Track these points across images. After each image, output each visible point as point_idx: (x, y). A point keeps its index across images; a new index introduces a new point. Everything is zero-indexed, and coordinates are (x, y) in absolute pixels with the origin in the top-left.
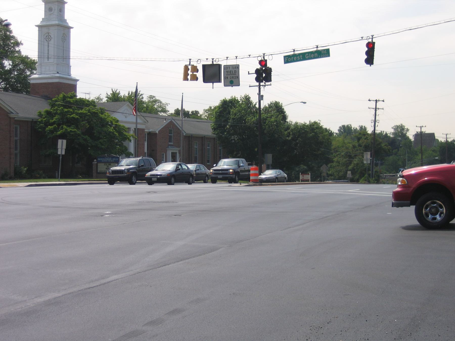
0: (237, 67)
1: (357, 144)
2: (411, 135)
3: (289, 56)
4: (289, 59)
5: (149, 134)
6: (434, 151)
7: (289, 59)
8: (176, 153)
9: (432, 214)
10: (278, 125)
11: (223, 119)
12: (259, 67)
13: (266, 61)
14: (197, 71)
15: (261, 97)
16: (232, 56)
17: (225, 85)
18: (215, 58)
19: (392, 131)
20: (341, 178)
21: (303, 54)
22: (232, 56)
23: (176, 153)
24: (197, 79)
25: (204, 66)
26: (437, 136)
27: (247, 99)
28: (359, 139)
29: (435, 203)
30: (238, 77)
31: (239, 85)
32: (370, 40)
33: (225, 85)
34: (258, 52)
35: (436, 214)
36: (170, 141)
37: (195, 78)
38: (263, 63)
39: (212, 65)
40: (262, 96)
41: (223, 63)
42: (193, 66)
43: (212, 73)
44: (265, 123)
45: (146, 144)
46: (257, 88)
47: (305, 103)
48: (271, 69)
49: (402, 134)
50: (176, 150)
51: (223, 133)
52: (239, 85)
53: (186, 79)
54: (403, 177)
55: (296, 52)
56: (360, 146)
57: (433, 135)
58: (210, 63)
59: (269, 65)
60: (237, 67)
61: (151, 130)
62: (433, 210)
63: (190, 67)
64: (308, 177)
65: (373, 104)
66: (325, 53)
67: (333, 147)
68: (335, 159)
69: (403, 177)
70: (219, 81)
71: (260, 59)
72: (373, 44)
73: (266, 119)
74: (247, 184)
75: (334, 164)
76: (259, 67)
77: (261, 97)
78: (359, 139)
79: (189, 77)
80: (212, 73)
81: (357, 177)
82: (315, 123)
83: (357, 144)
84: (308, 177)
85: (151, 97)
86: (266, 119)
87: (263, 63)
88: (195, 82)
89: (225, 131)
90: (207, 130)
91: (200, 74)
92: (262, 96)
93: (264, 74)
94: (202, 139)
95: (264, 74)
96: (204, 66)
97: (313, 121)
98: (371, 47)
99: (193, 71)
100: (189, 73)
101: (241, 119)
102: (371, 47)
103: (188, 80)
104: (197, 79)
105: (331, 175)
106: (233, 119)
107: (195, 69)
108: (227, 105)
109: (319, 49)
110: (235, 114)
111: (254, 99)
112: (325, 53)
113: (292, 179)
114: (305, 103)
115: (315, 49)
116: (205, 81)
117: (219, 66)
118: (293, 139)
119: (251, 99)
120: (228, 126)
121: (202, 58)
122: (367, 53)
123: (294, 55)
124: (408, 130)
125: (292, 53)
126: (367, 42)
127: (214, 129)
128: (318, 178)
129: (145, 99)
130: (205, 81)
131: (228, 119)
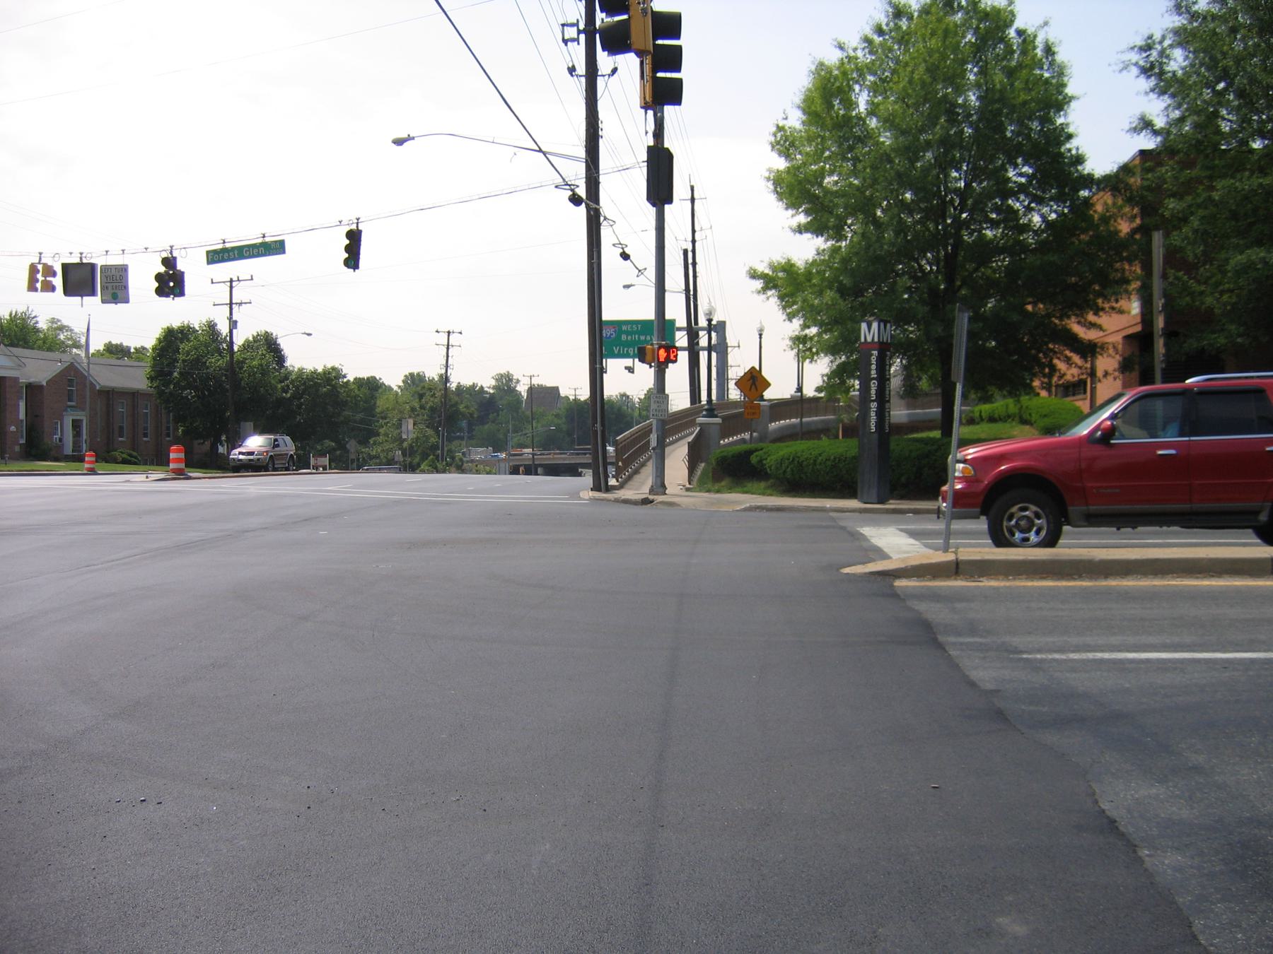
0: (123, 269)
1: (417, 405)
2: (522, 389)
3: (215, 252)
4: (216, 256)
5: (30, 387)
6: (557, 416)
7: (216, 256)
8: (81, 421)
9: (1022, 531)
10: (264, 371)
11: (165, 362)
12: (162, 269)
13: (175, 259)
14: (54, 274)
15: (233, 324)
16: (115, 248)
17: (103, 302)
18: (85, 251)
19: (493, 383)
20: (388, 464)
21: (240, 249)
22: (115, 248)
23: (81, 421)
24: (53, 289)
25: (66, 267)
26: (563, 393)
27: (211, 326)
28: (421, 396)
29: (1025, 509)
30: (126, 287)
31: (127, 301)
32: (354, 227)
33: (103, 302)
34: (161, 246)
35: (1029, 530)
36: (70, 400)
37: (50, 288)
38: (169, 262)
39: (81, 265)
40: (236, 322)
41: (100, 262)
42: (45, 265)
43: (79, 279)
44: (241, 368)
45: (22, 405)
46: (227, 308)
47: (309, 335)
48: (183, 273)
49: (509, 387)
50: (82, 416)
51: (167, 384)
52: (127, 301)
53: (32, 287)
54: (965, 461)
55: (228, 245)
56: (422, 407)
57: (556, 389)
58: (77, 260)
59: (180, 266)
60: (123, 269)
61: (32, 380)
62: (1023, 523)
63: (40, 267)
64: (325, 461)
65: (443, 339)
66: (276, 248)
67: (378, 410)
68: (382, 431)
69: (965, 461)
70: (93, 293)
71: (165, 255)
72: (359, 232)
73: (243, 362)
74: (162, 476)
75: (381, 439)
76: (162, 269)
77: (233, 324)
78: (421, 396)
79: (39, 285)
80: (79, 279)
81: (417, 460)
82: (333, 369)
83: (417, 405)
84: (325, 461)
85: (53, 321)
86: (243, 362)
87: (169, 262)
88: (50, 294)
89: (170, 382)
90: (138, 379)
91: (58, 281)
92: (236, 322)
93: (170, 282)
94: (134, 395)
95: (170, 282)
96: (66, 267)
97: (329, 366)
98: (354, 238)
99: (45, 275)
100: (38, 278)
101: (198, 362)
102: (354, 238)
103: (36, 290)
104: (53, 289)
105: (377, 457)
106: (184, 361)
107: (49, 271)
108: (173, 339)
109: (267, 239)
110: (188, 353)
111: (223, 328)
112: (276, 248)
113: (298, 463)
114: (309, 335)
115: (260, 240)
116: (67, 292)
117: (92, 267)
118: (293, 397)
119: (219, 327)
120: (175, 374)
121: (63, 250)
122: (348, 249)
123: (224, 250)
124: (518, 381)
125: (220, 246)
126: (348, 228)
127: (151, 379)
128: (343, 463)
129: (43, 325)
130: (67, 292)
131: (176, 360)
